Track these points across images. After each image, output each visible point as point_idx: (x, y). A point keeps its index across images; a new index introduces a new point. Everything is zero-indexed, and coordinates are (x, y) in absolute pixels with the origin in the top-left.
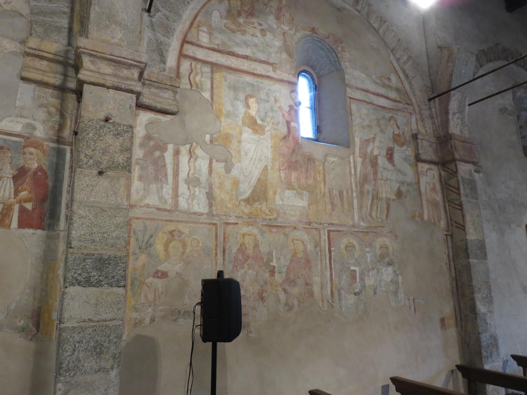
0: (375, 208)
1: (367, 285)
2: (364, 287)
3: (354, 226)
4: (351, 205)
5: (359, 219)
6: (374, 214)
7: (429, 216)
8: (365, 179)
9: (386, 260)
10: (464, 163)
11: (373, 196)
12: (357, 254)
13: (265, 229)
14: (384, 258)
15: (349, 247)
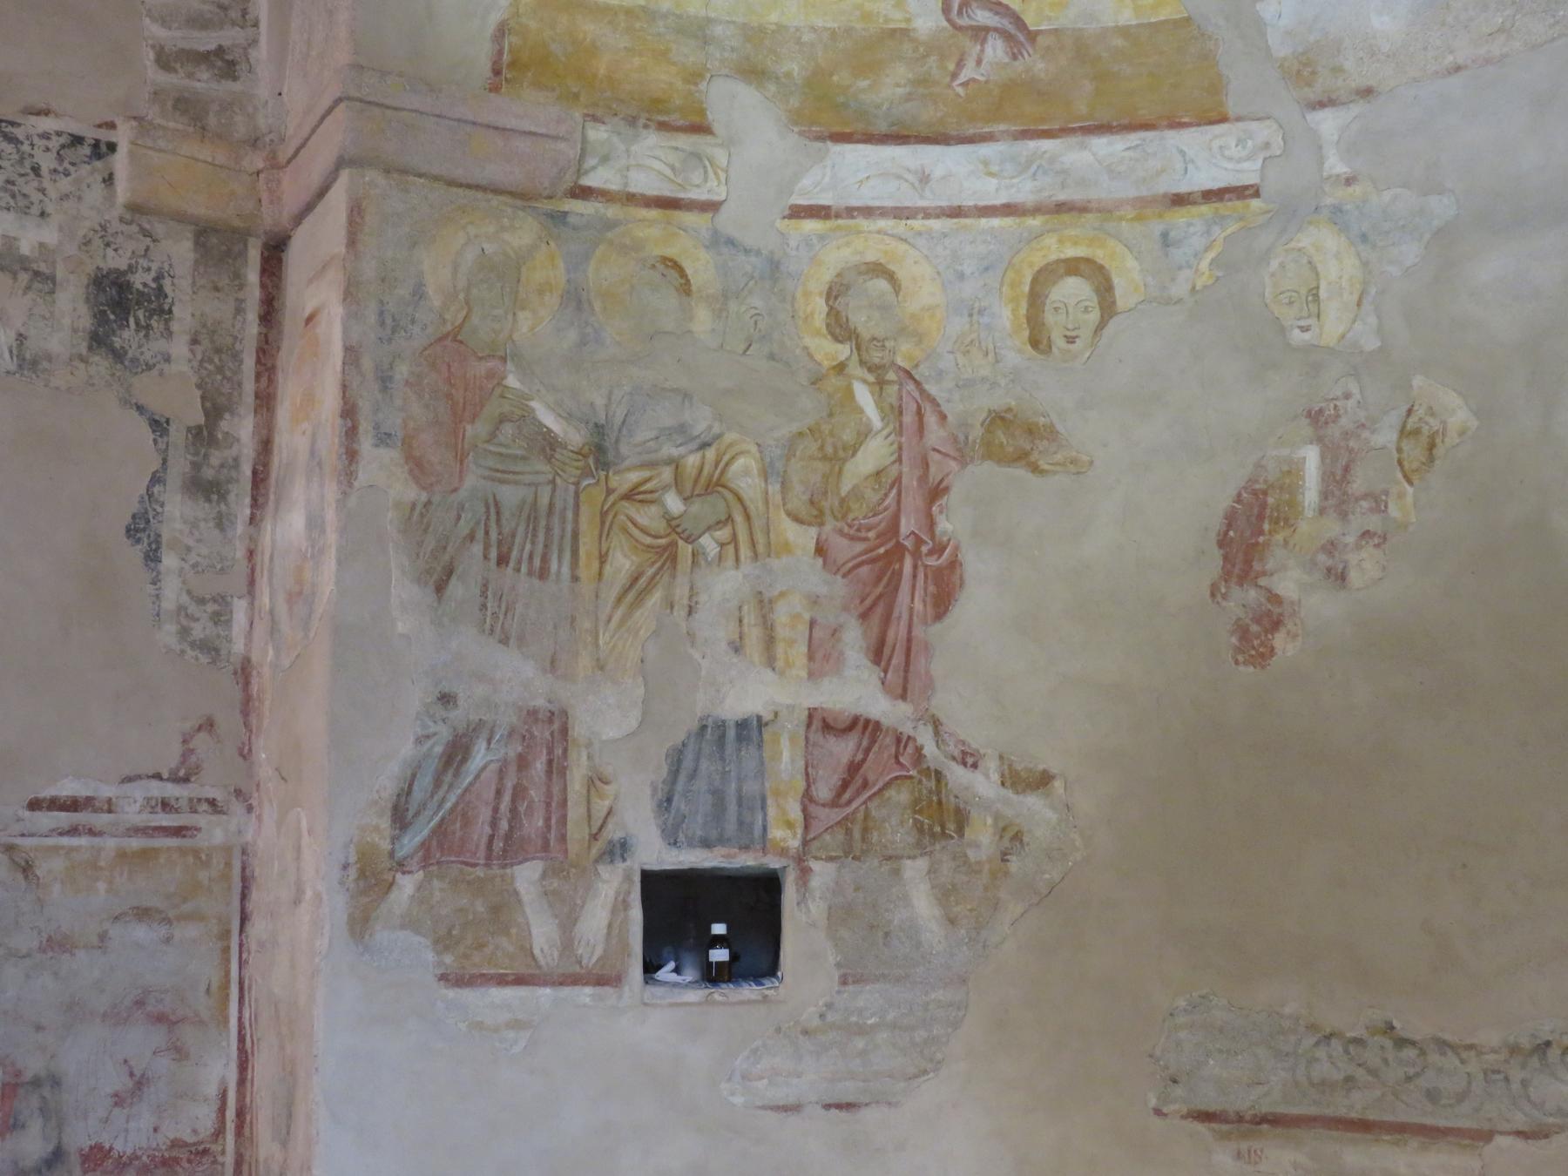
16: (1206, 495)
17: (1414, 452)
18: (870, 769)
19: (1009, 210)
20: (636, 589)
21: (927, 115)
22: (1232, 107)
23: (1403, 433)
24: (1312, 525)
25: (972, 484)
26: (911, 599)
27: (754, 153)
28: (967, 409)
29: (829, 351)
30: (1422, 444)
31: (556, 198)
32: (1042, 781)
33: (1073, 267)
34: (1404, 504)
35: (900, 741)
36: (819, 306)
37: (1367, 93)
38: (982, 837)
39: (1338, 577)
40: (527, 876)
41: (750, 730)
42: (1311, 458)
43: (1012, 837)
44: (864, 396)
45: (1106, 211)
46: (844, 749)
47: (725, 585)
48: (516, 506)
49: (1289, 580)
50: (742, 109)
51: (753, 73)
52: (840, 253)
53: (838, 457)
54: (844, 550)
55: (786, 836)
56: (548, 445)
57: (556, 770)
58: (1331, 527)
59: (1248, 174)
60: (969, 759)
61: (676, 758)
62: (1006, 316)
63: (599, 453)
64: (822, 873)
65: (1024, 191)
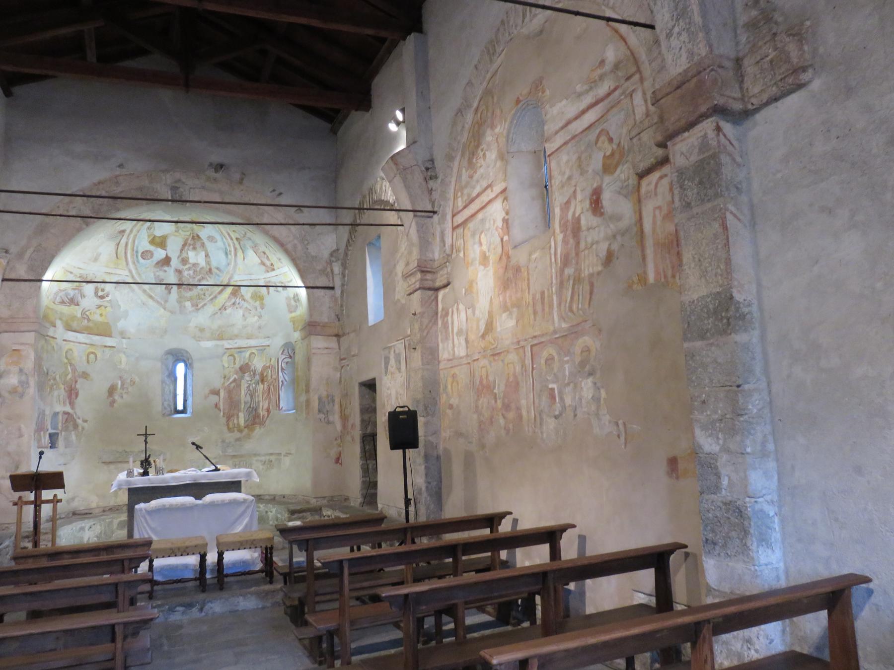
0: (576, 297)
1: (567, 405)
2: (564, 407)
3: (555, 332)
4: (551, 306)
5: (559, 320)
6: (575, 307)
7: (657, 273)
8: (566, 262)
9: (587, 368)
10: (686, 134)
11: (574, 280)
12: (556, 366)
13: (491, 359)
14: (585, 368)
15: (549, 360)
16: (106, 386)
18: (70, 419)
21: (78, 329)
24: (119, 390)
25: (80, 381)
26: (74, 396)
28: (80, 370)
29: (66, 361)
30: (133, 383)
33: (92, 353)
34: (130, 389)
38: (80, 428)
39: (122, 397)
43: (83, 428)
46: (66, 416)
47: (56, 393)
49: (116, 397)
51: (61, 319)
52: (67, 346)
62: (85, 358)
64: (63, 433)
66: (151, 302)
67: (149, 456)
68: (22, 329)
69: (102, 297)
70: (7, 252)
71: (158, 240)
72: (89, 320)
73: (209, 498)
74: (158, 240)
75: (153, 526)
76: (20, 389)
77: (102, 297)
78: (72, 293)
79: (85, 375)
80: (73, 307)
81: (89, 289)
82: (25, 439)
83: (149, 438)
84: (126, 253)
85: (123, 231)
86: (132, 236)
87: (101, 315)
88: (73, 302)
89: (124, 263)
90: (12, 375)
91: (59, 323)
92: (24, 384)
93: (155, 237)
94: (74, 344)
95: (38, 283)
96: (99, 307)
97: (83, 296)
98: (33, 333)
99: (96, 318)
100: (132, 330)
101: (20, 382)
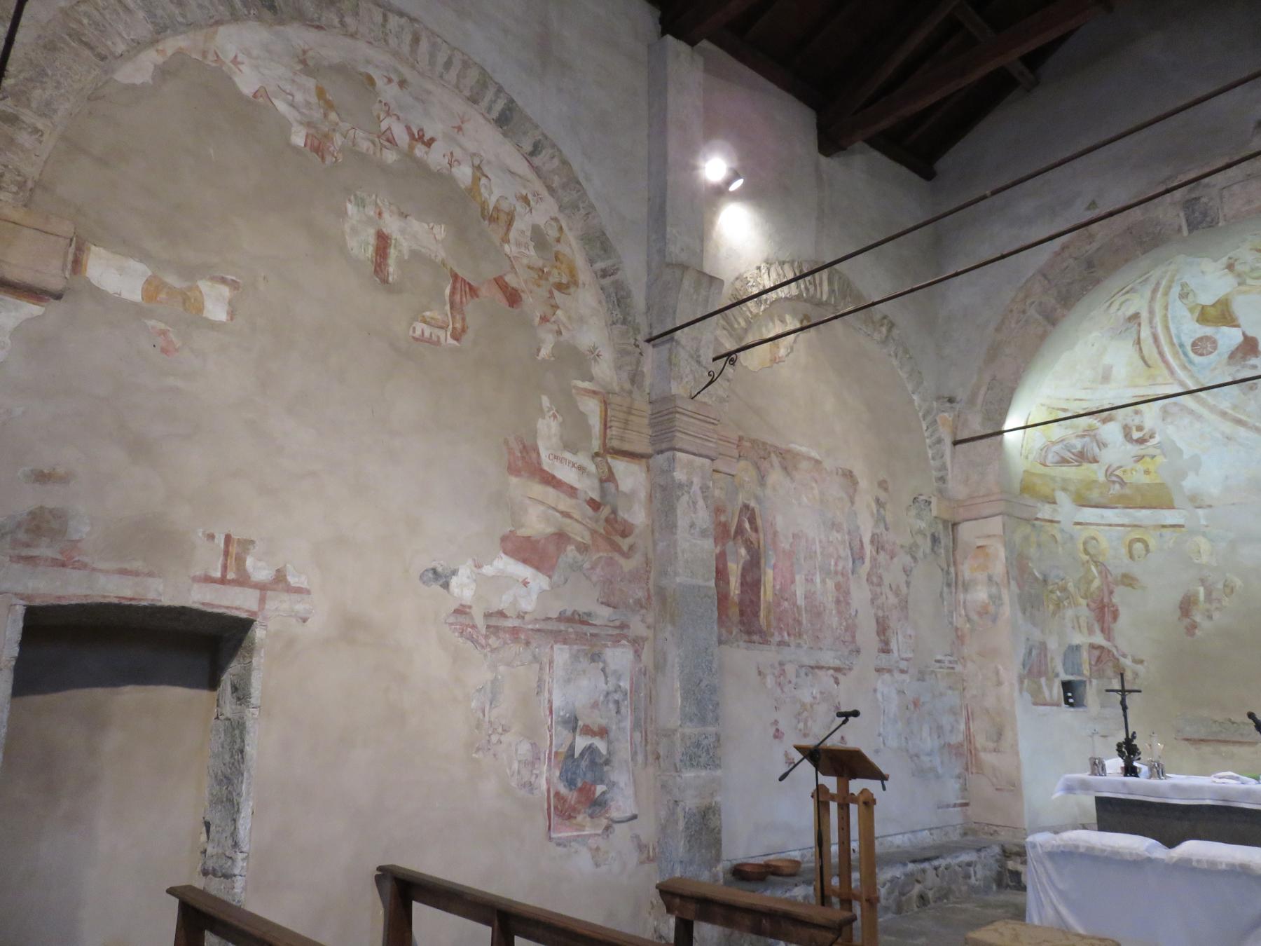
16: (1176, 597)
17: (1228, 591)
19: (1122, 525)
20: (1054, 614)
22: (1176, 505)
23: (1225, 586)
26: (1108, 618)
27: (1066, 510)
29: (1086, 558)
30: (1229, 589)
31: (1031, 521)
32: (1141, 662)
33: (1139, 540)
34: (1226, 602)
35: (1109, 651)
36: (1081, 547)
37: (1210, 506)
39: (1210, 617)
40: (1043, 680)
41: (1078, 647)
42: (1202, 590)
44: (1093, 568)
45: (1146, 527)
46: (1097, 653)
47: (1069, 613)
48: (1036, 593)
49: (1198, 618)
50: (1063, 498)
51: (1064, 489)
53: (1090, 582)
54: (1093, 605)
55: (1086, 672)
56: (1036, 579)
57: (1046, 656)
58: (1208, 606)
59: (1181, 522)
60: (1124, 656)
61: (1065, 655)
63: (1045, 581)
64: (1094, 682)
65: (1126, 521)
66: (1242, 432)
67: (1134, 737)
68: (987, 512)
69: (1141, 441)
70: (951, 400)
71: (1212, 312)
72: (1123, 483)
73: (1192, 849)
74: (1212, 312)
75: (1061, 886)
76: (992, 609)
77: (1141, 441)
78: (1078, 444)
79: (1128, 580)
80: (1086, 465)
81: (1111, 431)
82: (1005, 689)
83: (1131, 700)
84: (1161, 354)
85: (1136, 316)
86: (1158, 320)
87: (1147, 472)
88: (1083, 457)
89: (1166, 372)
90: (979, 588)
91: (1061, 497)
92: (996, 599)
93: (1203, 307)
94: (1105, 528)
95: (998, 438)
96: (1140, 458)
97: (1102, 445)
98: (999, 519)
99: (1137, 477)
100: (1215, 491)
101: (990, 597)
